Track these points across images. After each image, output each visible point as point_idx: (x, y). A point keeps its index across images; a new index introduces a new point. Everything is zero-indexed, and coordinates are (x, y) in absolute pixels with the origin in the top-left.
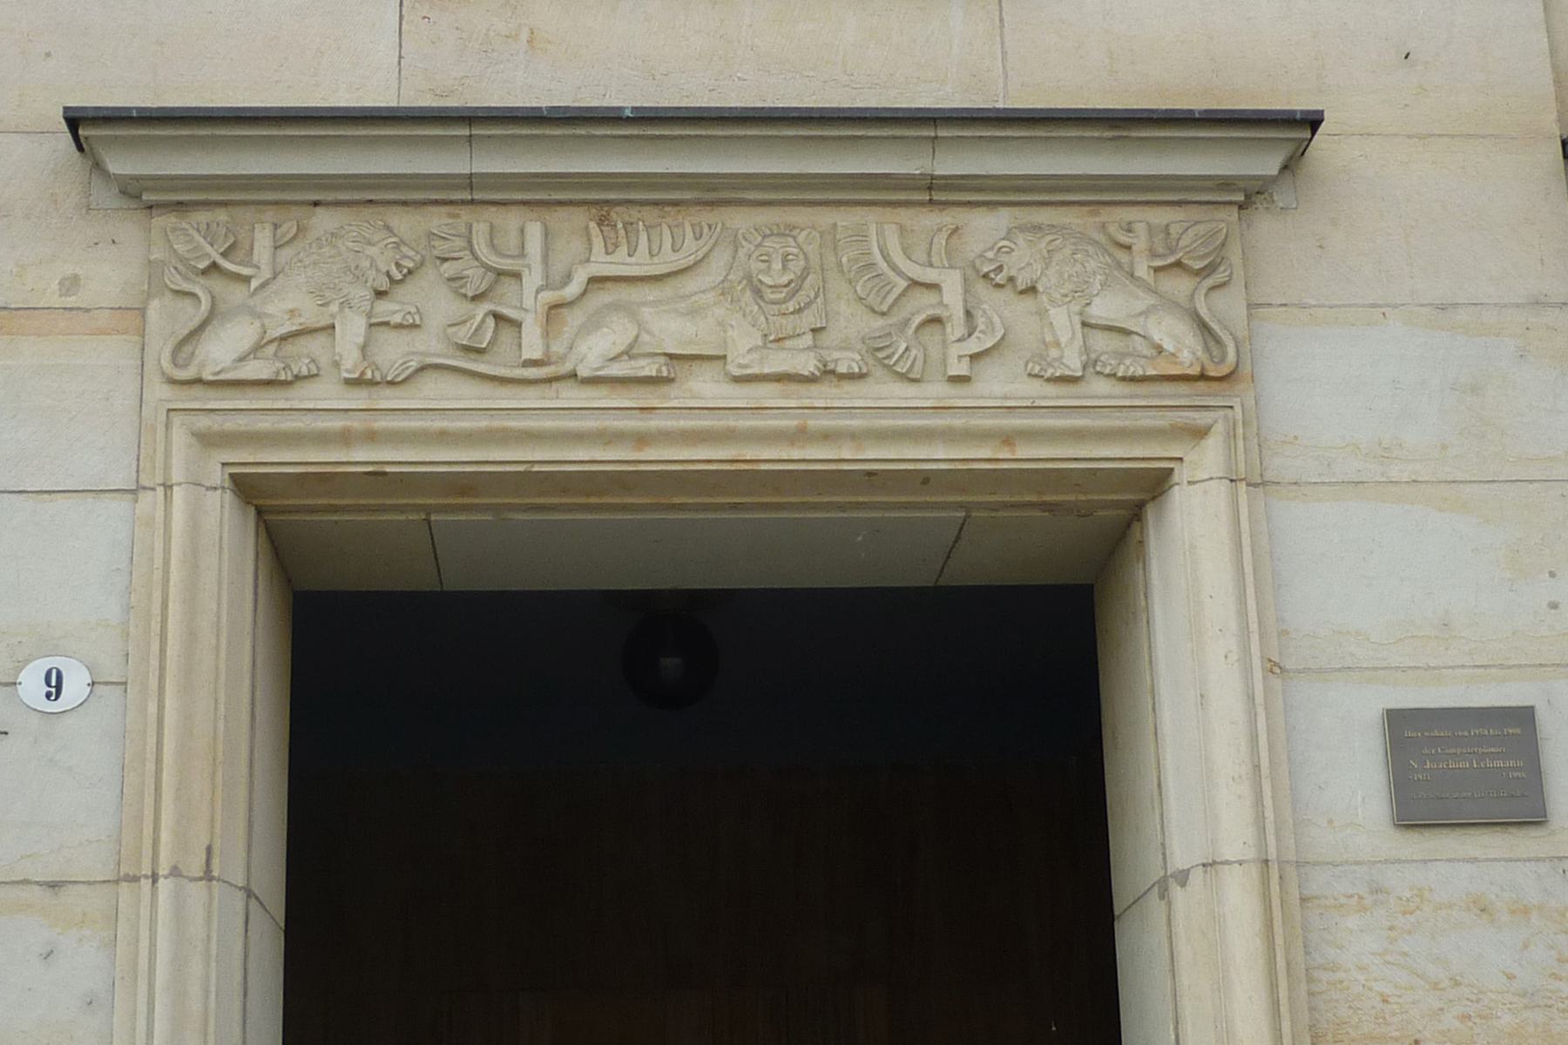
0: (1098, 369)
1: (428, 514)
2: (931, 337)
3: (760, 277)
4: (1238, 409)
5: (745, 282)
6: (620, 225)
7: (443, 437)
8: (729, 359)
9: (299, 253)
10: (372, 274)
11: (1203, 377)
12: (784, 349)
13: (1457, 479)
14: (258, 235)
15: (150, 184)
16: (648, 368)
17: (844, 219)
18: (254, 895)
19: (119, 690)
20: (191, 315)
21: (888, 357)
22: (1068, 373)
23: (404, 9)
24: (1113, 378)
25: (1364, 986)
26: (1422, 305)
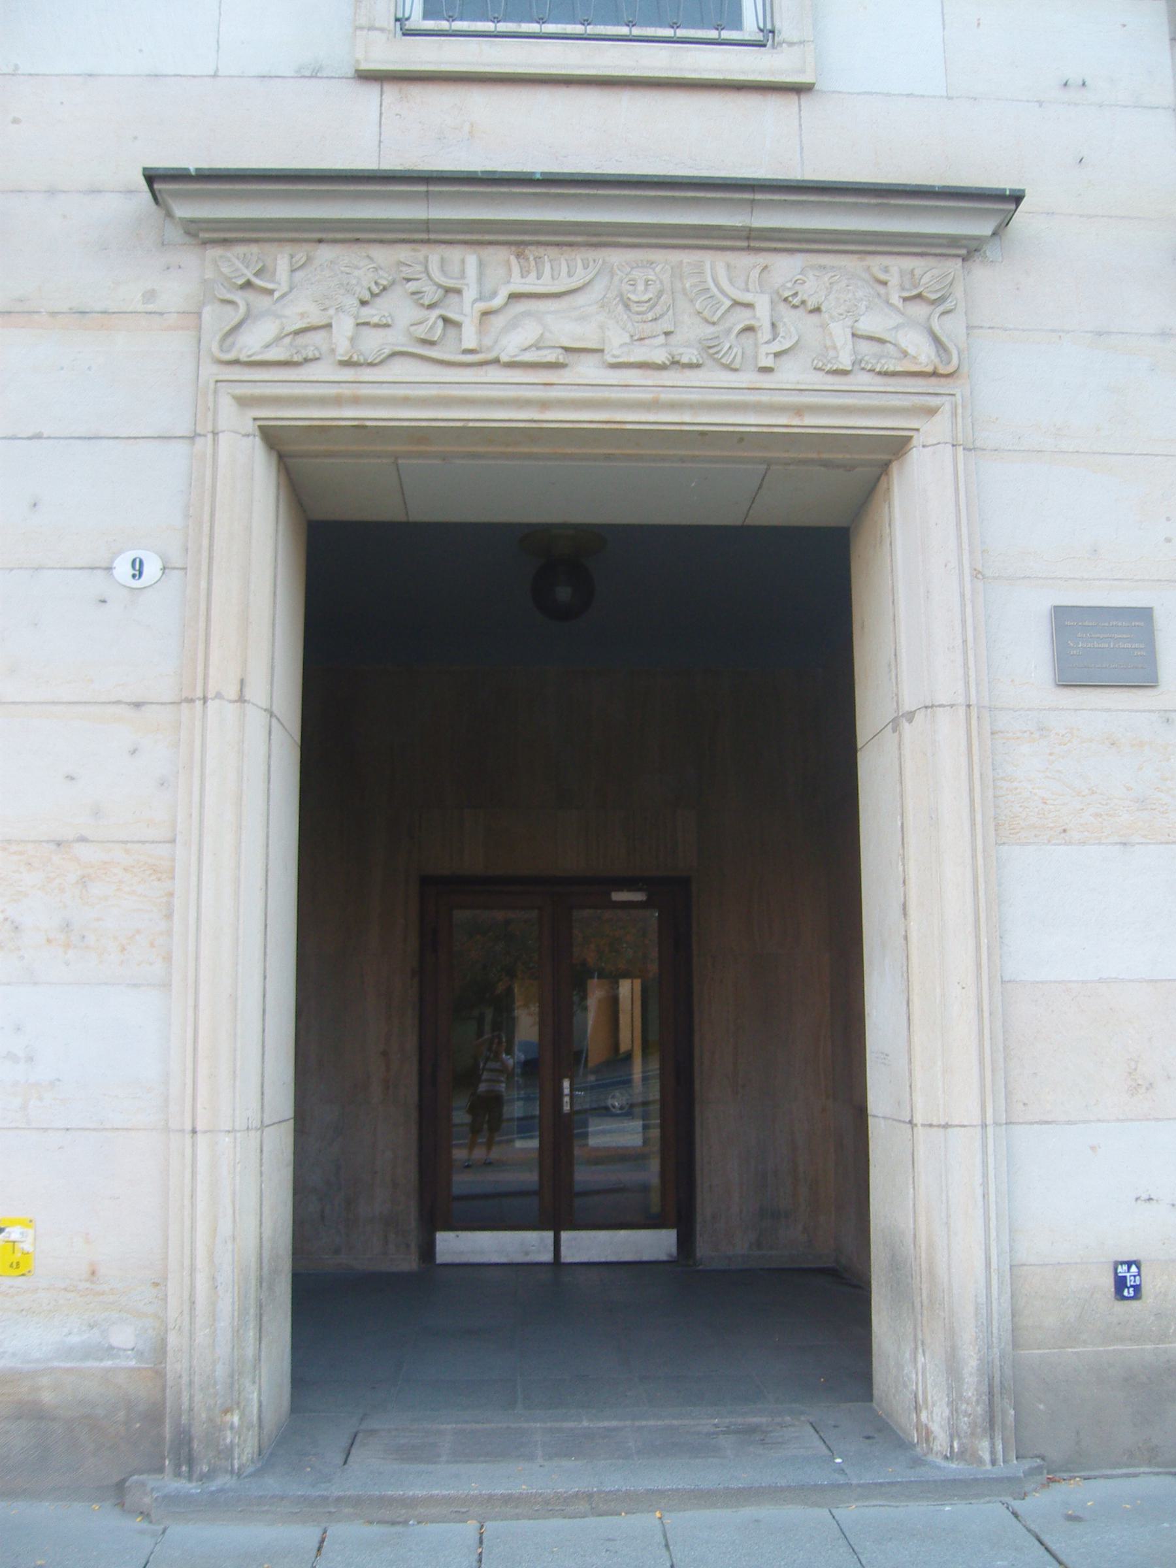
0: (863, 365)
1: (396, 458)
2: (747, 339)
3: (629, 295)
4: (958, 396)
5: (618, 299)
6: (531, 258)
7: (406, 401)
8: (606, 352)
9: (308, 275)
10: (358, 289)
11: (935, 374)
12: (644, 345)
13: (1106, 451)
14: (279, 262)
15: (204, 226)
16: (550, 356)
17: (687, 258)
18: (275, 716)
19: (182, 572)
20: (234, 316)
21: (717, 353)
22: (841, 367)
23: (383, 108)
24: (918, 301)
25: (1031, 792)
26: (1087, 332)
